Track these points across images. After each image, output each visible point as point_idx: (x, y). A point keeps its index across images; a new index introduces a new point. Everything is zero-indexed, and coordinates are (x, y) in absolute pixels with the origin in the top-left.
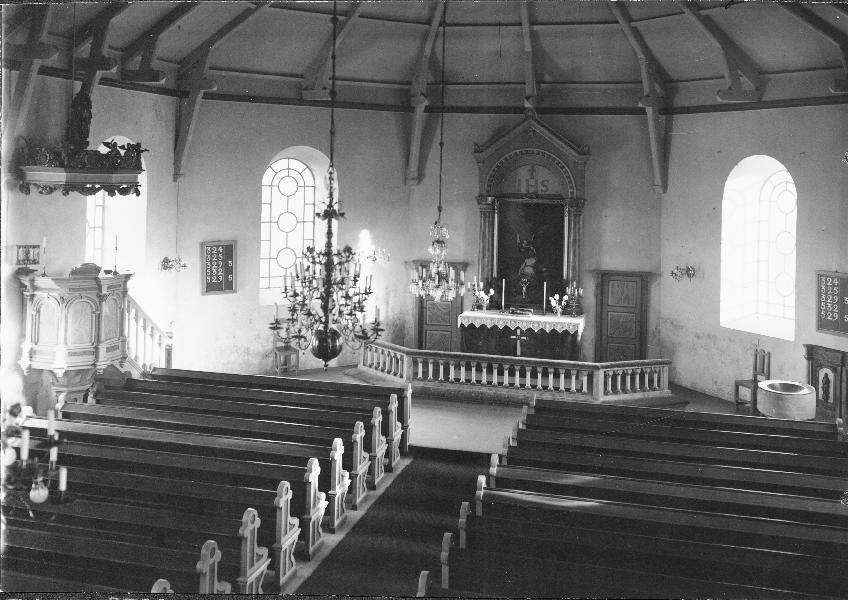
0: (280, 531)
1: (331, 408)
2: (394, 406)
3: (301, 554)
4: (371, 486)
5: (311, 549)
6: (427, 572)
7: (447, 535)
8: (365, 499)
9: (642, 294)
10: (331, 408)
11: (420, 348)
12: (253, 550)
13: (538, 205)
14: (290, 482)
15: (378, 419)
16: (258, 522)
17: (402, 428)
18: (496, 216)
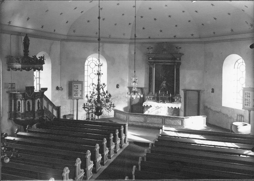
0: (87, 165)
1: (106, 130)
2: (123, 129)
3: (102, 163)
4: (121, 147)
5: (97, 170)
6: (128, 177)
7: (134, 167)
8: (114, 156)
9: (74, 40)
10: (106, 130)
11: (132, 112)
12: (79, 170)
13: (169, 65)
14: (80, 158)
15: (117, 133)
16: (80, 162)
17: (125, 136)
18: (154, 68)
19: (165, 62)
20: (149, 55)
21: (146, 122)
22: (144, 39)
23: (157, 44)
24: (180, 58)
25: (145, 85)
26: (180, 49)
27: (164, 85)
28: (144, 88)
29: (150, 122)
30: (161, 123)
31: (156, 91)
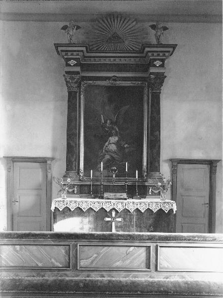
19: (115, 79)
20: (70, 49)
21: (75, 265)
22: (39, 245)
23: (93, 20)
24: (163, 61)
25: (54, 149)
26: (165, 32)
27: (113, 147)
28: (49, 159)
29: (94, 265)
30: (143, 265)
31: (90, 164)
